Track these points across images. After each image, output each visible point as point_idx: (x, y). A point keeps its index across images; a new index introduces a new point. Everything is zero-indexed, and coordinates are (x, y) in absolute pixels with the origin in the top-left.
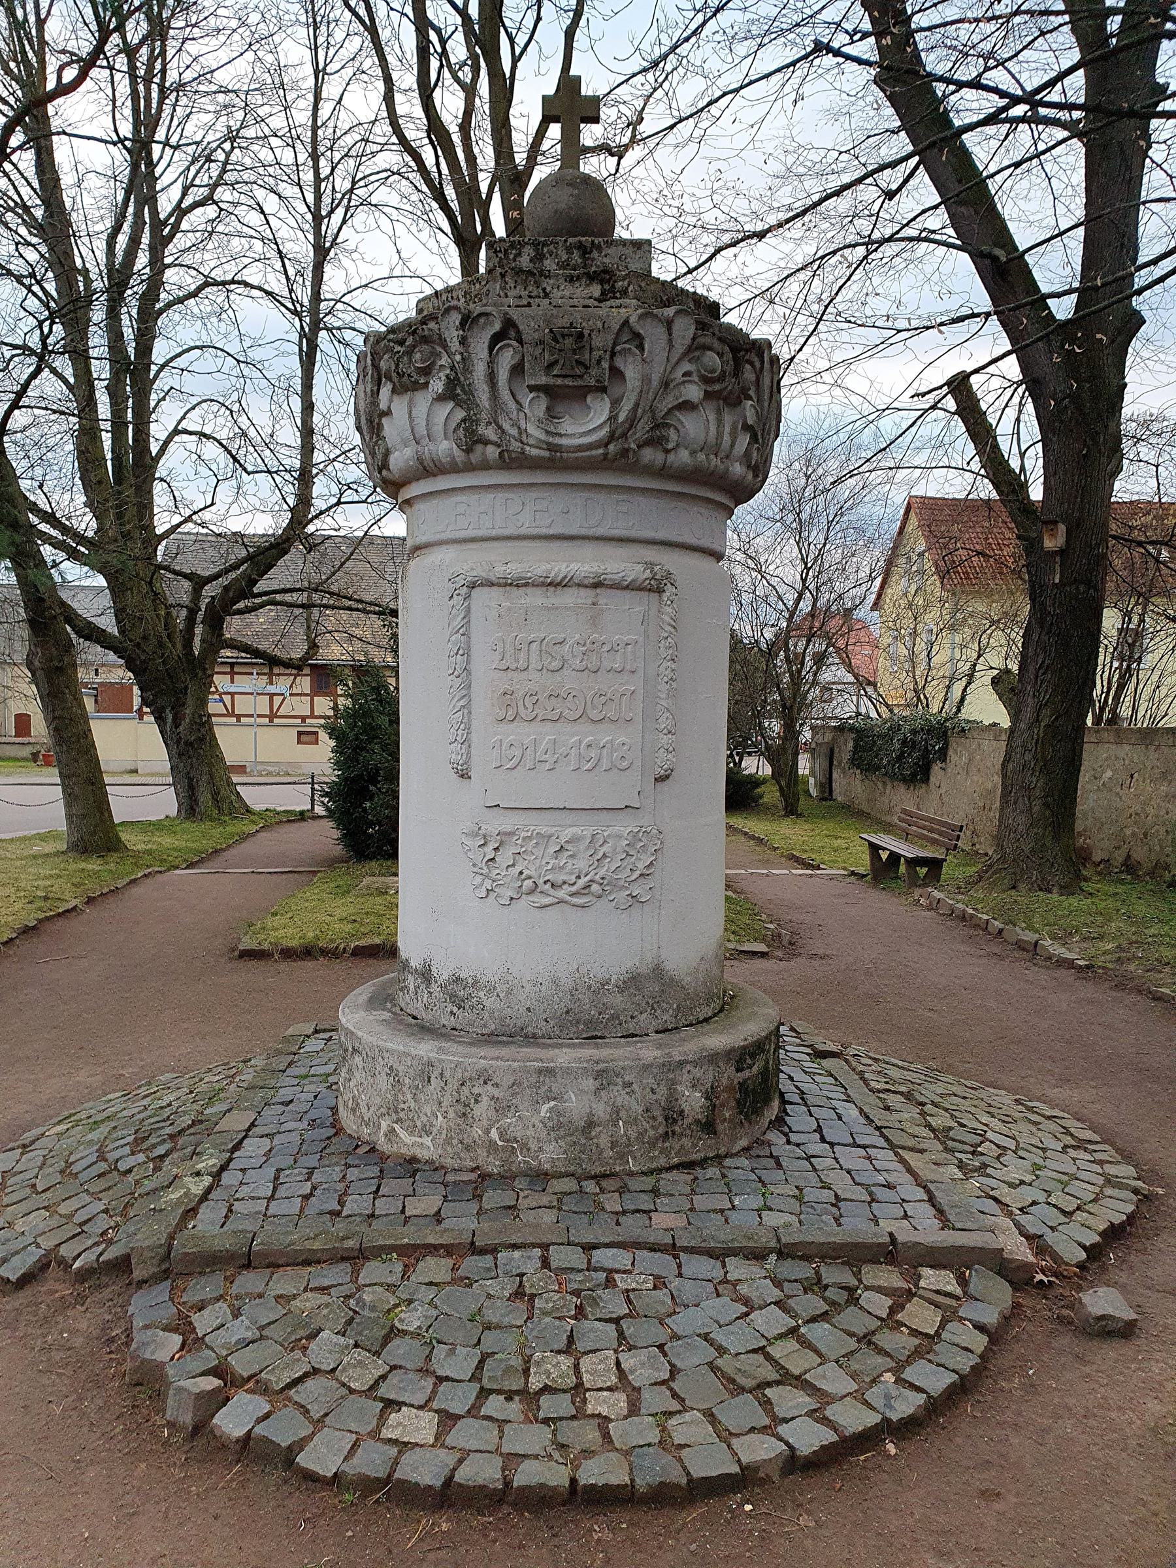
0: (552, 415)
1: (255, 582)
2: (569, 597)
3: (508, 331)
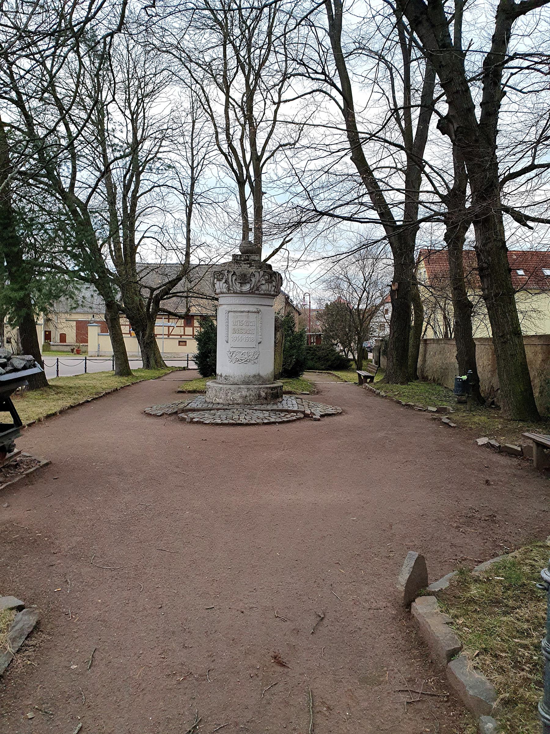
0: (241, 286)
1: (171, 289)
2: (244, 314)
3: (234, 274)
